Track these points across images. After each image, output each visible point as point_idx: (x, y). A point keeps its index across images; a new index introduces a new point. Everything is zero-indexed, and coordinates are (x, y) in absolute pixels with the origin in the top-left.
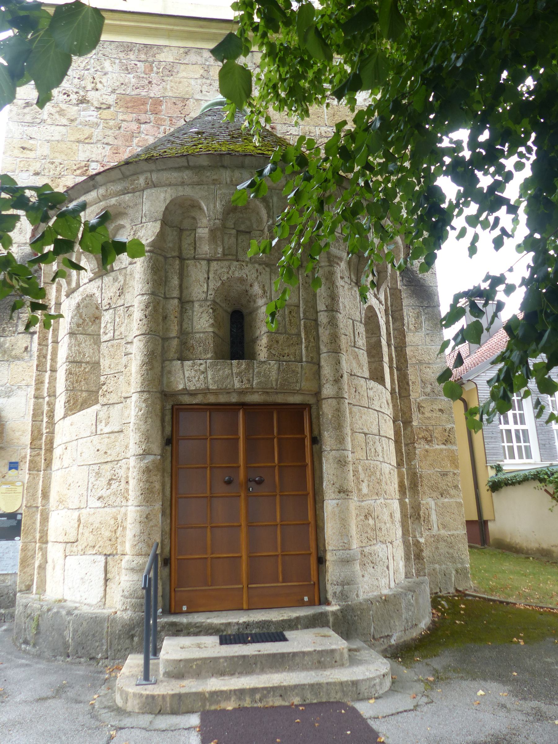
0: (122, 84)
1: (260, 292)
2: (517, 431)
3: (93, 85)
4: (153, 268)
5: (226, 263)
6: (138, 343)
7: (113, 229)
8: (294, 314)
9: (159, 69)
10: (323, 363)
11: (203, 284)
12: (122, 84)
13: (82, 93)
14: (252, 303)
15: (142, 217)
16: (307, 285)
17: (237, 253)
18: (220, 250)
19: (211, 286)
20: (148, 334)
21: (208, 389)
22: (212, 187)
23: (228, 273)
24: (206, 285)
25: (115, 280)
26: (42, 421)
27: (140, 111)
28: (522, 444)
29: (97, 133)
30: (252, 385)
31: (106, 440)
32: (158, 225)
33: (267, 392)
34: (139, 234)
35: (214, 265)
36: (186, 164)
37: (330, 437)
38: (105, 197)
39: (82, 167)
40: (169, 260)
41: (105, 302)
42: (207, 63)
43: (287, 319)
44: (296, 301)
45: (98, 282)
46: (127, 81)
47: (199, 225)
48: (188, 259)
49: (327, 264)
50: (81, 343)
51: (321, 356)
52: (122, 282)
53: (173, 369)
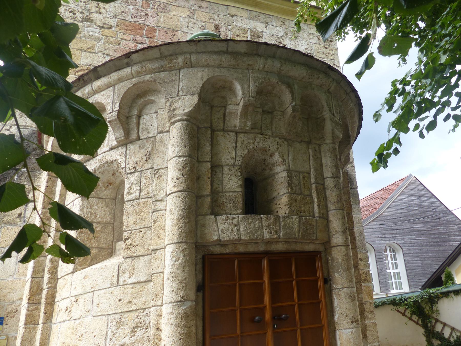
0: (123, 12)
1: (280, 160)
2: (394, 273)
3: (97, 9)
4: (189, 135)
5: (252, 136)
6: (175, 199)
7: (141, 104)
8: (306, 179)
9: (154, 6)
10: (331, 218)
11: (231, 152)
12: (123, 12)
13: (86, 14)
14: (268, 171)
15: (178, 91)
16: (316, 157)
17: (261, 128)
18: (249, 124)
19: (239, 153)
20: (186, 191)
21: (240, 239)
22: (246, 71)
23: (253, 143)
24: (234, 152)
25: (142, 147)
26: (43, 277)
27: (137, 34)
28: (397, 281)
29: (99, 46)
30: (279, 236)
31: (130, 291)
32: (195, 100)
33: (289, 242)
34: (176, 105)
35: (242, 137)
36: (225, 49)
37: (342, 277)
38: (138, 74)
39: (84, 70)
40: (202, 131)
41: (130, 166)
42: (193, 8)
43: (302, 183)
44: (308, 169)
45: (123, 150)
46: (127, 10)
47: (229, 103)
48: (218, 131)
49: (332, 142)
50: (93, 206)
51: (330, 213)
52: (150, 149)
53: (207, 222)
